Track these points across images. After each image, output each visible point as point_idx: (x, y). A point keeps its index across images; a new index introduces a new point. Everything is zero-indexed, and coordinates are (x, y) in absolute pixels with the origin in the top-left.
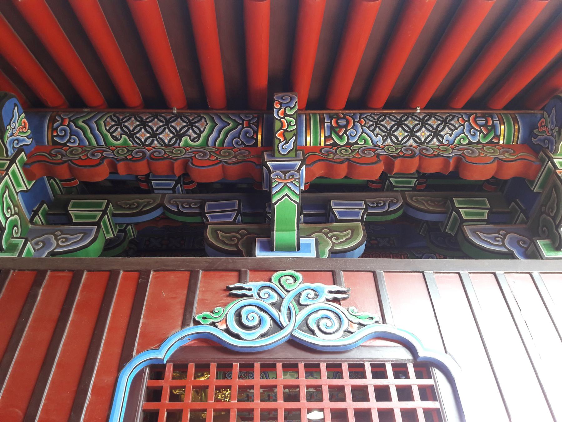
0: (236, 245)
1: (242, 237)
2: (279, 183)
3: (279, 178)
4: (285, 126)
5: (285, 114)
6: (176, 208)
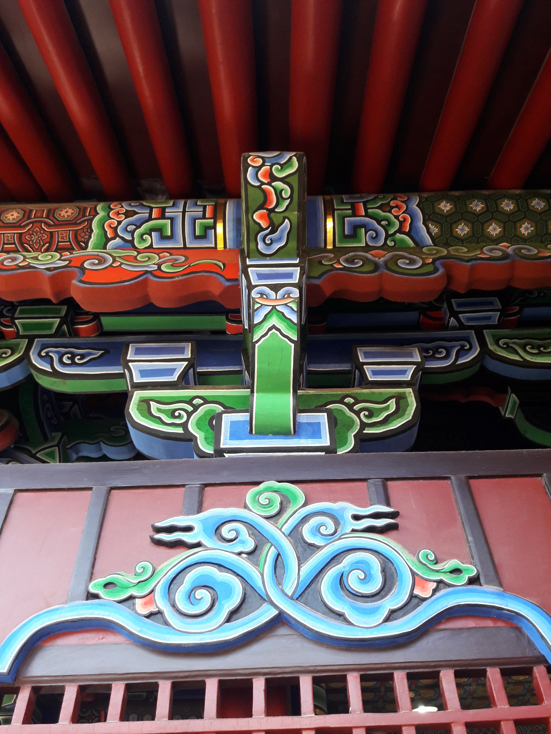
0: (184, 425)
1: (196, 408)
2: (262, 305)
3: (264, 298)
4: (271, 203)
5: (273, 178)
6: (49, 366)
